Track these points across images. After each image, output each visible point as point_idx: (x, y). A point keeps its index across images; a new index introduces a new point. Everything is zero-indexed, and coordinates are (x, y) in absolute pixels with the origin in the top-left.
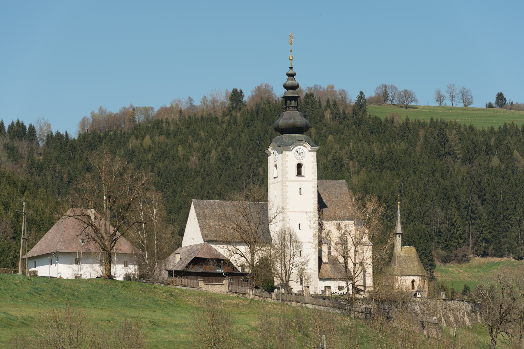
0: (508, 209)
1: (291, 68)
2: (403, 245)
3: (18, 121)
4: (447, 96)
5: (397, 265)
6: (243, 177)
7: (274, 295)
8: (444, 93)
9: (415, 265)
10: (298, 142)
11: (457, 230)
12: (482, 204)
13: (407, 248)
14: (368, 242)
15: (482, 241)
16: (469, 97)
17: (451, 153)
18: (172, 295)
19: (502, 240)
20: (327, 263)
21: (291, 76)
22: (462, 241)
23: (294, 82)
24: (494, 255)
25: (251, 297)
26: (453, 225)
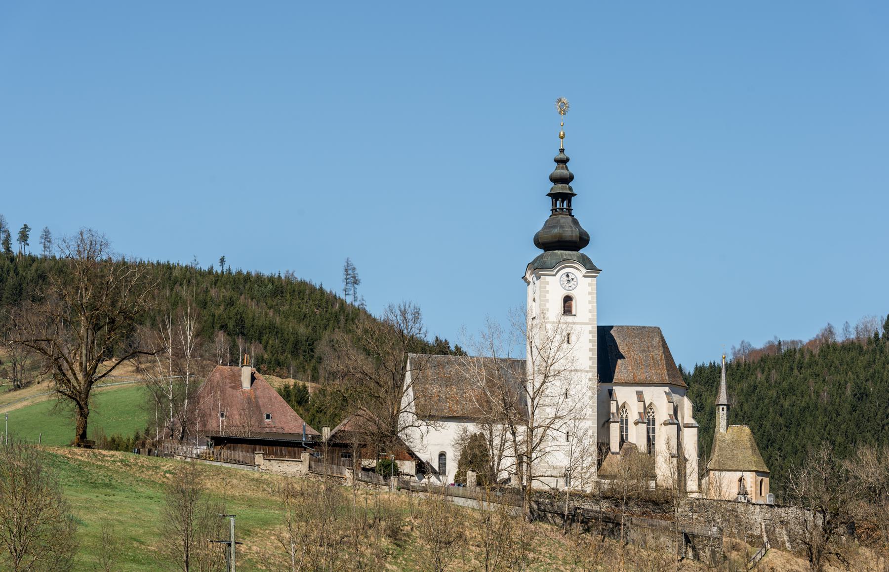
1: (562, 151)
5: (716, 454)
6: (879, 416)
9: (748, 454)
14: (693, 421)
20: (618, 453)
21: (562, 162)
23: (565, 172)
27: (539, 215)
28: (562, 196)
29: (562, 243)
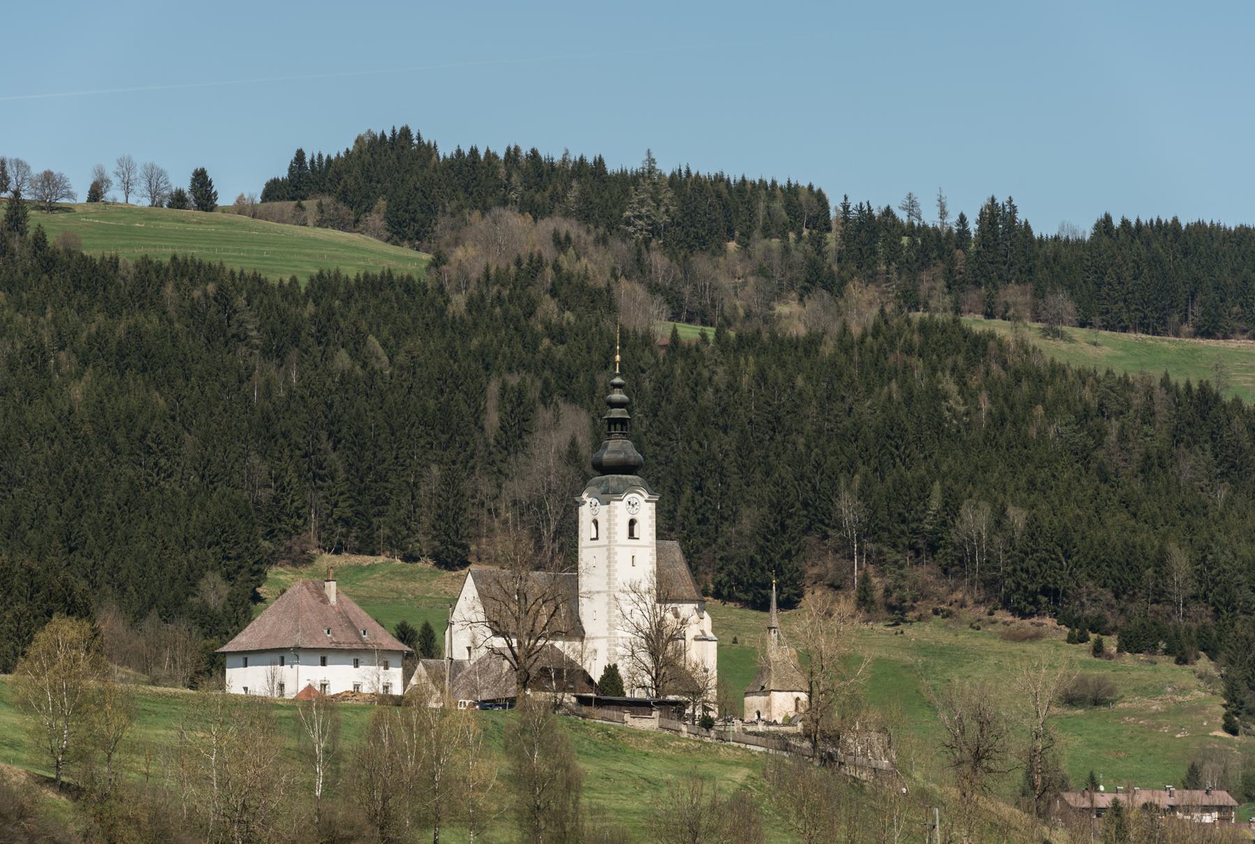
0: (384, 461)
4: (116, 181)
7: (712, 733)
8: (110, 173)
10: (631, 488)
11: (293, 501)
12: (334, 449)
15: (336, 522)
16: (162, 185)
17: (242, 336)
18: (610, 736)
19: (374, 520)
22: (300, 522)
24: (359, 551)
25: (686, 735)
26: (283, 490)
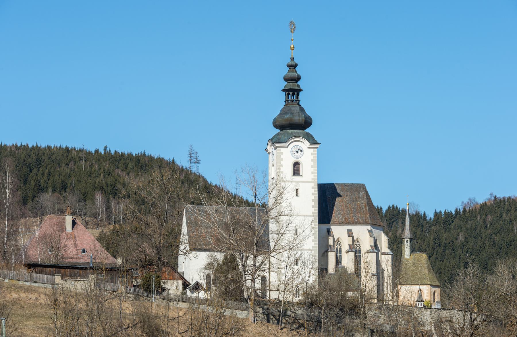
1: (292, 59)
2: (413, 250)
3: (393, 206)
13: (417, 255)
14: (388, 250)
21: (293, 67)
27: (278, 102)
28: (293, 90)
29: (293, 124)
